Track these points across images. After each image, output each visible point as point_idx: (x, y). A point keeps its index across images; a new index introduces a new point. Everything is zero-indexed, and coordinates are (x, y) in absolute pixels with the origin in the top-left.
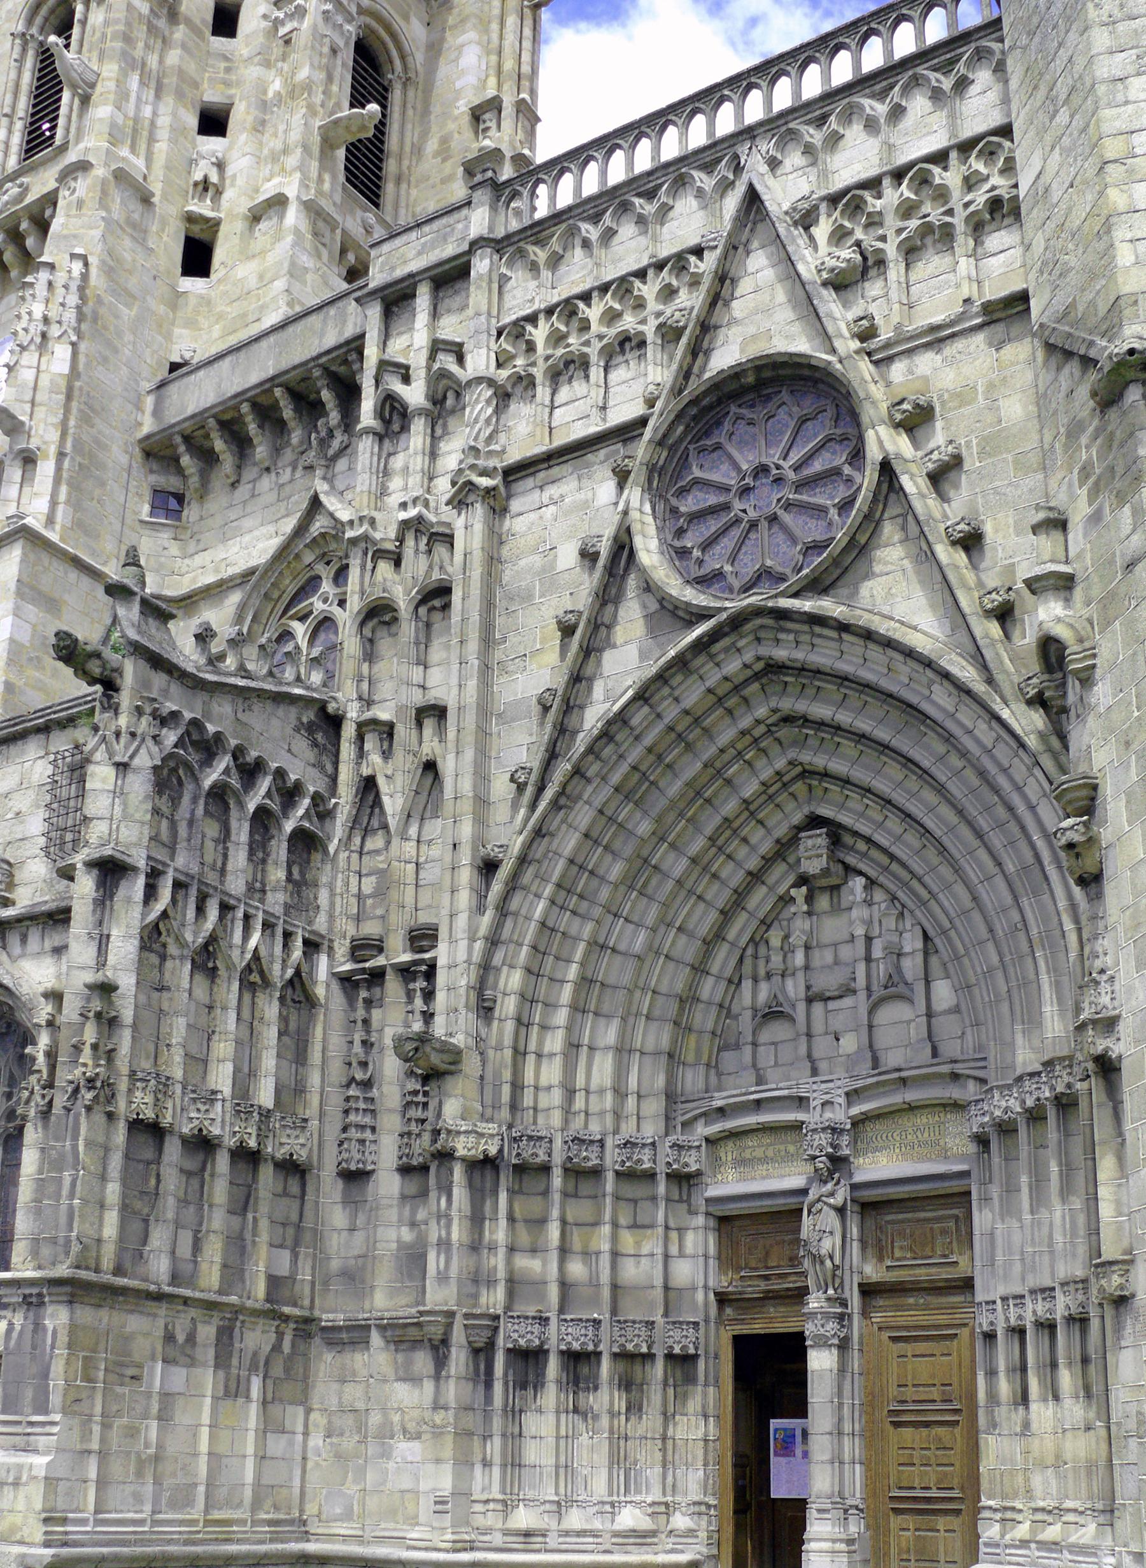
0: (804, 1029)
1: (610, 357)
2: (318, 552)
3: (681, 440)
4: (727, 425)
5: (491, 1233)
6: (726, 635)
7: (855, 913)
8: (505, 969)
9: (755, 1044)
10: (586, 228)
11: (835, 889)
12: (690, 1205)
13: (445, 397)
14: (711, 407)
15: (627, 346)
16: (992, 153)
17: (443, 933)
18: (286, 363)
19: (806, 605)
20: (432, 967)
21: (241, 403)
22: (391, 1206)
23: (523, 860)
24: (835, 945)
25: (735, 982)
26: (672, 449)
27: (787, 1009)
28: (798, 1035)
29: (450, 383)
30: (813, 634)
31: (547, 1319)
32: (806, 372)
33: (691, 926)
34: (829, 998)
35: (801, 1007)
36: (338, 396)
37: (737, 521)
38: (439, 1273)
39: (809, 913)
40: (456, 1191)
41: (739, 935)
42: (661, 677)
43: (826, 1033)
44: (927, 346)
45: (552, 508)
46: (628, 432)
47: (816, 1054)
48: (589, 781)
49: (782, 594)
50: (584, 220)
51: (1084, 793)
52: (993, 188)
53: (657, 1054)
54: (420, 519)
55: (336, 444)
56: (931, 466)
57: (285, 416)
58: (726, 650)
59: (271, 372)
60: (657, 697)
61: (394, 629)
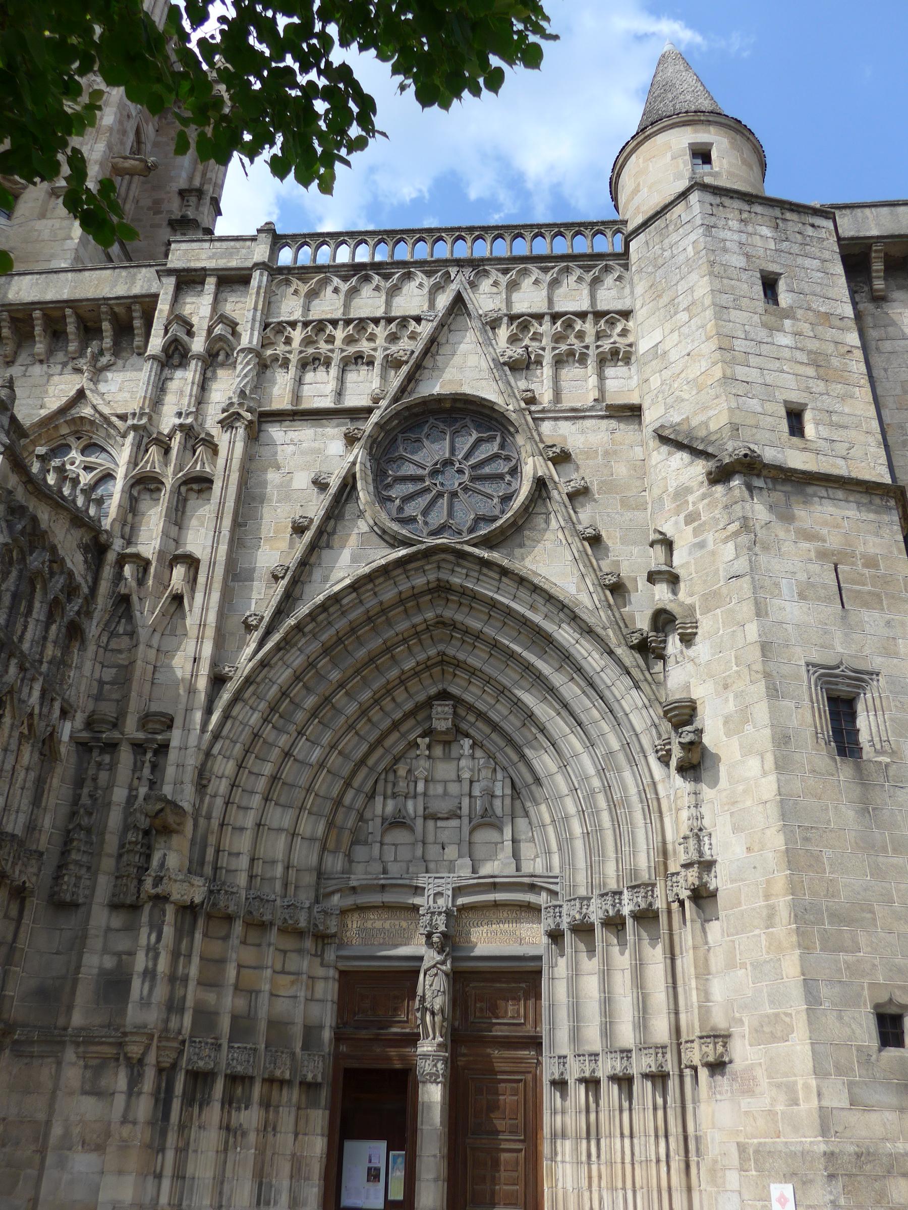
0: (420, 837)
1: (346, 365)
2: (73, 429)
3: (394, 429)
4: (426, 429)
5: (184, 968)
6: (418, 560)
7: (463, 763)
8: (220, 757)
9: (382, 844)
10: (336, 281)
11: (447, 744)
12: (323, 959)
13: (217, 354)
14: (416, 415)
15: (360, 361)
16: (613, 324)
17: (178, 722)
18: (79, 294)
19: (485, 554)
20: (163, 748)
21: (35, 309)
22: (97, 936)
23: (248, 681)
24: (445, 782)
25: (371, 796)
26: (387, 433)
27: (408, 821)
28: (416, 841)
29: (225, 346)
30: (480, 572)
31: (220, 1046)
32: (487, 412)
33: (347, 751)
34: (439, 819)
35: (419, 822)
36: (114, 329)
37: (427, 490)
38: (142, 998)
39: (429, 757)
40: (166, 929)
41: (377, 763)
42: (369, 578)
43: (435, 843)
44: (567, 418)
45: (292, 447)
46: (359, 414)
47: (428, 857)
48: (304, 635)
49: (466, 542)
50: (337, 276)
51: (687, 711)
52: (614, 343)
53: (312, 839)
54: (191, 427)
55: (104, 360)
56: (570, 489)
57: (68, 330)
58: (416, 569)
59: (65, 297)
60: (363, 589)
61: (155, 496)
